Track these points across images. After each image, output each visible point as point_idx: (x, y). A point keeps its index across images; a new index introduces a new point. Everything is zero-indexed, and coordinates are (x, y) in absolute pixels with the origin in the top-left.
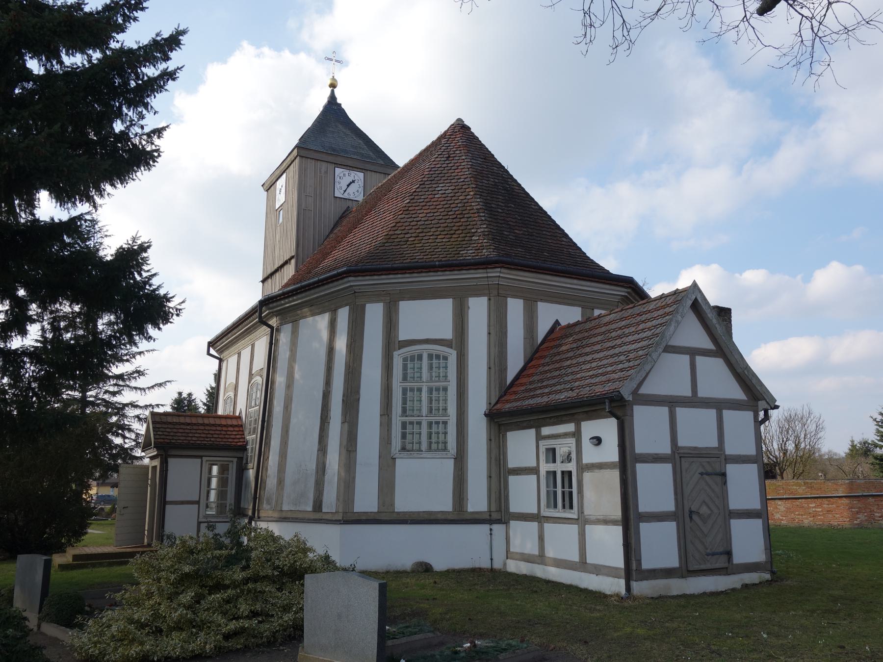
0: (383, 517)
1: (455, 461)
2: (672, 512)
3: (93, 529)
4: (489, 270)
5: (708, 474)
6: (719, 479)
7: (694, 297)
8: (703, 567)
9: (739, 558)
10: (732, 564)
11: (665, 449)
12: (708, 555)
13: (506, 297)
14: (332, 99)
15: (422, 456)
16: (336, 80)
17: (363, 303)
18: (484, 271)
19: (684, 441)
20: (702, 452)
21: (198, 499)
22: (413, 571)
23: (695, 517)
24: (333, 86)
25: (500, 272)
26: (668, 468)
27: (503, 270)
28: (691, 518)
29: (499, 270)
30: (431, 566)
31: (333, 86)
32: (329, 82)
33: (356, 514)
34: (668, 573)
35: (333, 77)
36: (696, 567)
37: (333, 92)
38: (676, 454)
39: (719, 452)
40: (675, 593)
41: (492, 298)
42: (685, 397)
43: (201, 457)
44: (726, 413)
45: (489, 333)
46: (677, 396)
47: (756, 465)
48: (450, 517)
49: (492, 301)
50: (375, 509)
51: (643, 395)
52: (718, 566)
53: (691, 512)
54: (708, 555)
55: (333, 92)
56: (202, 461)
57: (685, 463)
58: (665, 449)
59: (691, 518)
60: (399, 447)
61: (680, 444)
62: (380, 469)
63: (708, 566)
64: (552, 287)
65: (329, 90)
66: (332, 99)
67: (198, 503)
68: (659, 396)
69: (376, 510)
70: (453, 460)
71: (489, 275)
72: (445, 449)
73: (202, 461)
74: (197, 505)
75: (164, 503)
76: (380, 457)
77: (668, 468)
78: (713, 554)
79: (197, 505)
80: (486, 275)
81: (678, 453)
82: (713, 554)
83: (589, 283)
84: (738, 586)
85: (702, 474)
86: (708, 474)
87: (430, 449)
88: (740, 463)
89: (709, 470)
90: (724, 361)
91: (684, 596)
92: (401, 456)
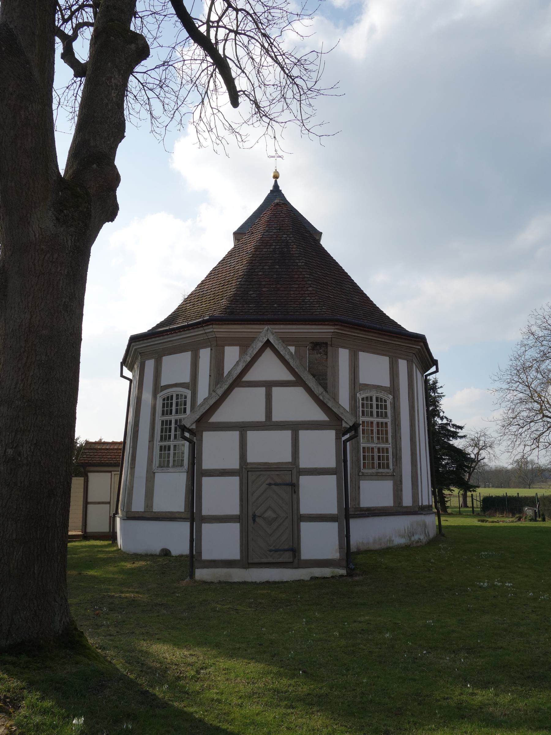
0: (147, 515)
1: (187, 474)
2: (236, 515)
3: (455, 511)
4: (205, 328)
5: (276, 484)
6: (289, 489)
7: (266, 339)
8: (264, 560)
9: (306, 553)
10: (299, 559)
11: (235, 464)
12: (270, 551)
13: (224, 346)
14: (276, 186)
15: (169, 471)
16: (278, 172)
17: (144, 360)
18: (201, 329)
19: (251, 458)
20: (272, 467)
21: (109, 501)
22: (160, 556)
23: (257, 520)
24: (276, 177)
25: (212, 328)
26: (235, 481)
27: (214, 326)
28: (254, 520)
29: (211, 326)
30: (170, 551)
31: (276, 177)
32: (272, 175)
33: (133, 513)
34: (229, 564)
35: (276, 170)
36: (256, 560)
37: (276, 182)
38: (244, 469)
39: (291, 466)
40: (236, 580)
41: (213, 348)
42: (257, 422)
43: (111, 472)
44: (303, 434)
45: (210, 376)
46: (252, 422)
47: (336, 476)
48: (183, 516)
49: (213, 351)
50: (142, 510)
51: (213, 423)
52: (281, 560)
53: (254, 517)
54: (270, 551)
55: (276, 182)
56: (111, 474)
57: (252, 476)
58: (235, 464)
59: (254, 520)
60: (157, 464)
61: (249, 460)
62: (147, 480)
63: (270, 560)
64: (176, 341)
65: (273, 180)
66: (276, 186)
67: (109, 503)
68: (230, 423)
69: (143, 510)
70: (186, 473)
71: (206, 331)
72: (182, 465)
73: (111, 474)
74: (109, 505)
75: (86, 503)
76: (147, 471)
77: (235, 481)
78: (276, 551)
79: (109, 505)
80: (203, 332)
81: (245, 468)
82: (276, 551)
83: (294, 327)
84: (307, 578)
85: (270, 484)
86: (276, 484)
87: (174, 466)
88: (316, 475)
89: (278, 481)
90: (305, 389)
91: (245, 583)
92: (158, 471)
